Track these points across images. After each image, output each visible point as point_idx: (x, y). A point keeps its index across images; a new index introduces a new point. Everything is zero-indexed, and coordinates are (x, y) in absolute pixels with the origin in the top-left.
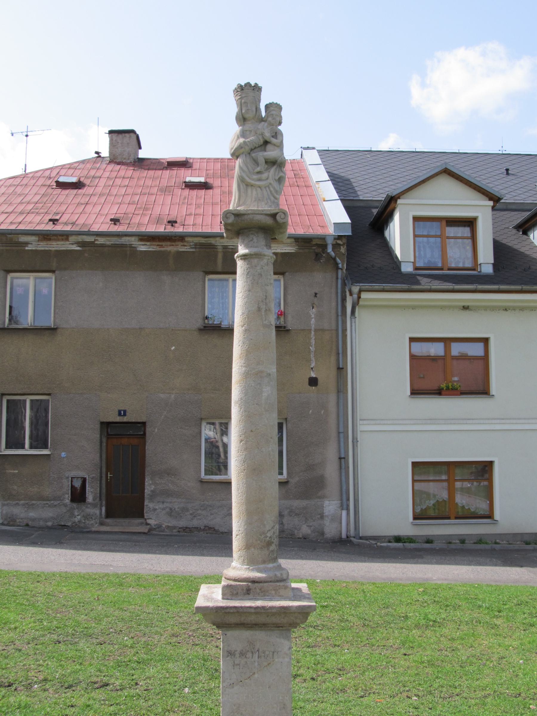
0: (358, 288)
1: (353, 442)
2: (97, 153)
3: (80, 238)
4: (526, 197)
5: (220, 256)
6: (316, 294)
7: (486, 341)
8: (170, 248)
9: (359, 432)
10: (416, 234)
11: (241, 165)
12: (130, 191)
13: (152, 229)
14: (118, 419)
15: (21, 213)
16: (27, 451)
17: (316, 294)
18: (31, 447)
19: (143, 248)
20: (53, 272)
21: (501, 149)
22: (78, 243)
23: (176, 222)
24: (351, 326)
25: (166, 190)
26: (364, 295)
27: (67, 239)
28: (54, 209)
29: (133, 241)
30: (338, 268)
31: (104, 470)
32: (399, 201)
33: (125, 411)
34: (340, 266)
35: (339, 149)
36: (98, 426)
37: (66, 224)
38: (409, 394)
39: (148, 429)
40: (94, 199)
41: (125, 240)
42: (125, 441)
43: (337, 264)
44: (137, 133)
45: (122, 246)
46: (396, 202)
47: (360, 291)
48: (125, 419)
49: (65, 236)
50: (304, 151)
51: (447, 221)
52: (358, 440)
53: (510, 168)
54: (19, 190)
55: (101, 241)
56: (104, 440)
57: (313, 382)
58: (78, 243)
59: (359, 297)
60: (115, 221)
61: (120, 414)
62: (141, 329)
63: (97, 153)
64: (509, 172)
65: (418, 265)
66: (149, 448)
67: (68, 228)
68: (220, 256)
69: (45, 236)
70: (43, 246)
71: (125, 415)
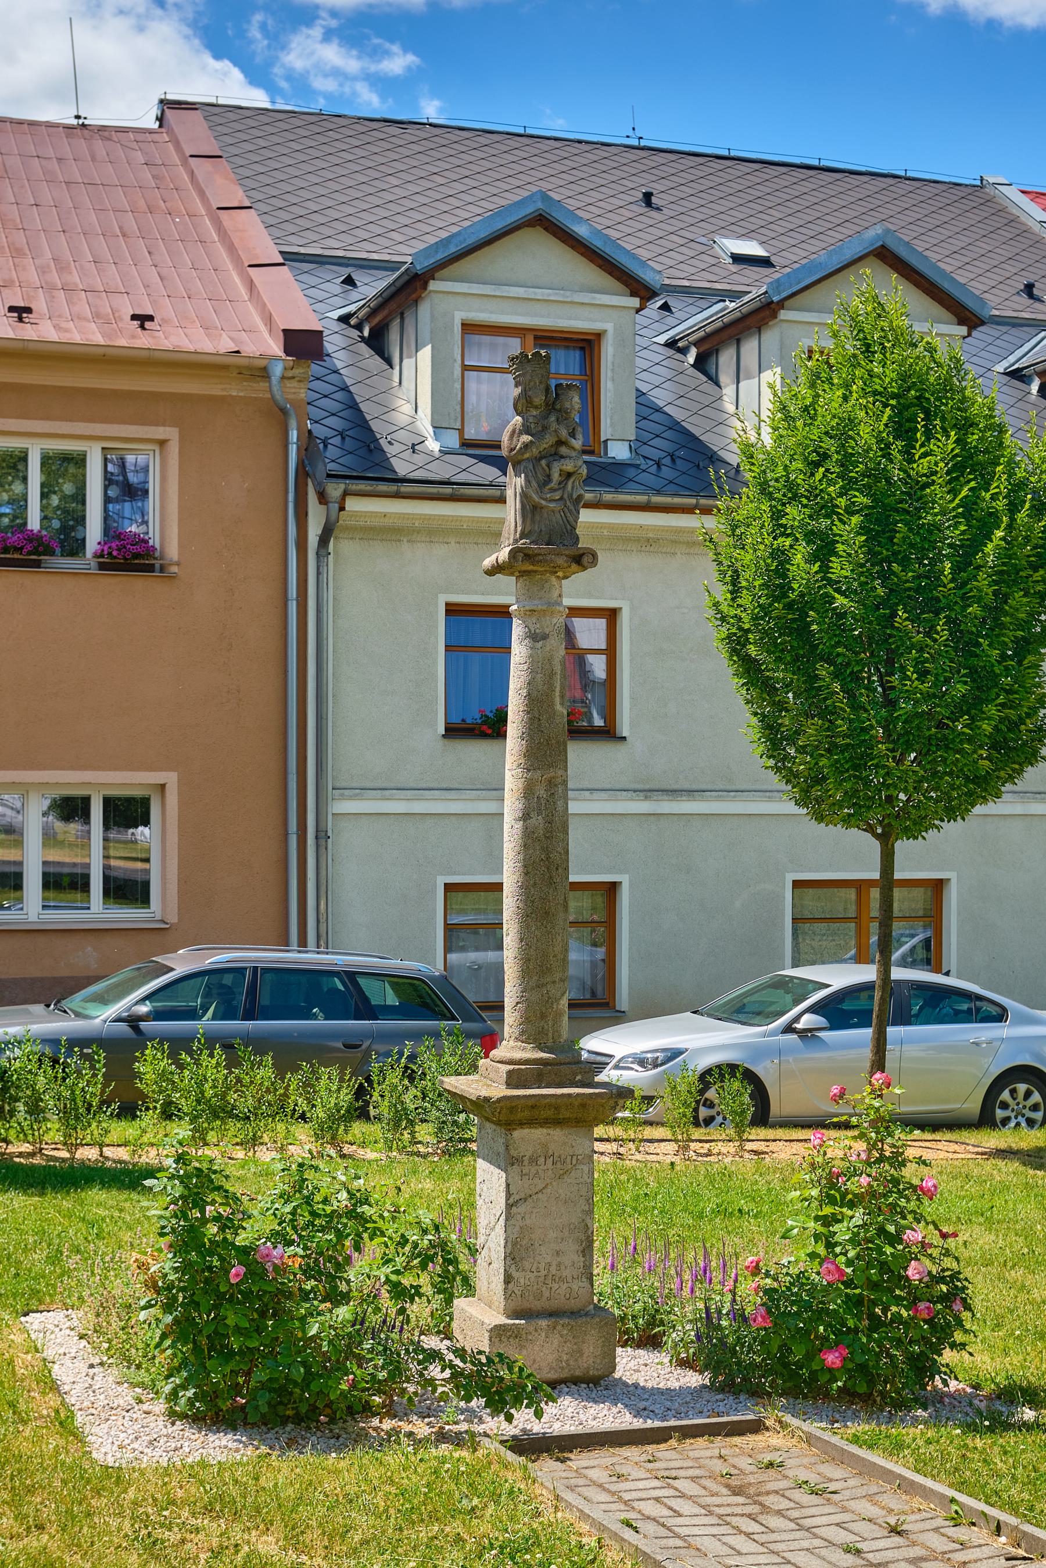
0: (342, 487)
1: (317, 838)
4: (693, 270)
7: (611, 615)
9: (330, 817)
10: (466, 363)
11: (518, 427)
21: (631, 133)
24: (318, 573)
26: (353, 505)
32: (433, 285)
35: (244, 104)
38: (442, 730)
46: (425, 286)
47: (346, 494)
50: (168, 112)
51: (536, 338)
52: (330, 834)
53: (656, 187)
59: (342, 508)
64: (654, 200)
65: (471, 433)
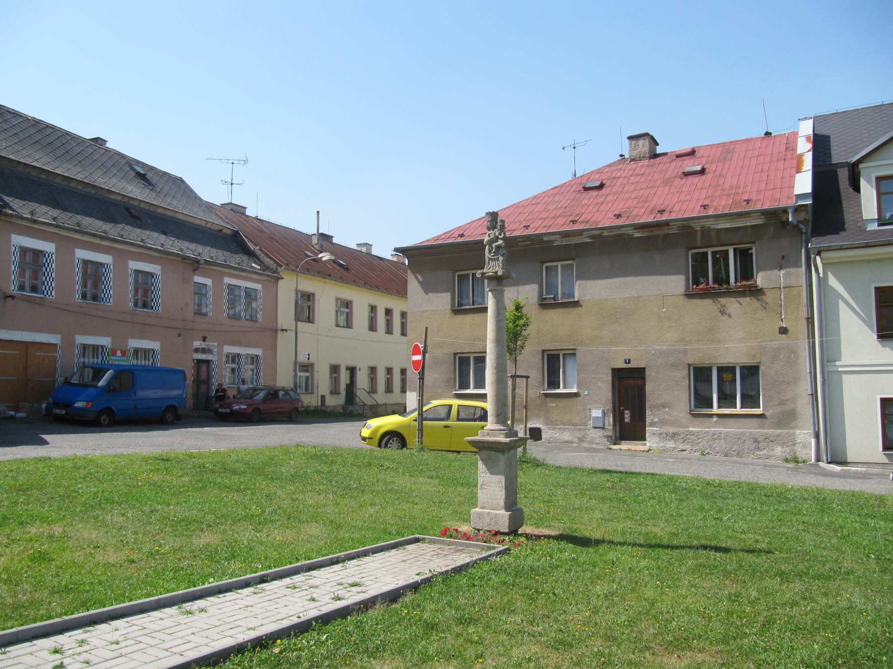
2: (621, 156)
3: (591, 233)
5: (699, 235)
6: (783, 257)
8: (660, 232)
12: (639, 186)
13: (644, 220)
14: (625, 366)
15: (553, 218)
16: (738, 410)
17: (783, 257)
18: (742, 407)
19: (637, 235)
20: (574, 259)
22: (590, 237)
23: (664, 211)
25: (668, 182)
27: (581, 234)
28: (577, 212)
29: (630, 231)
30: (802, 233)
31: (617, 404)
33: (629, 360)
34: (804, 230)
36: (610, 372)
37: (582, 222)
39: (647, 373)
40: (610, 198)
41: (622, 231)
42: (631, 382)
43: (801, 230)
44: (651, 134)
45: (622, 235)
48: (630, 366)
49: (580, 233)
54: (556, 199)
55: (606, 233)
56: (617, 382)
57: (784, 331)
58: (590, 237)
60: (618, 216)
61: (626, 362)
62: (638, 297)
63: (621, 156)
66: (649, 387)
67: (581, 227)
68: (699, 235)
69: (566, 235)
70: (566, 242)
71: (629, 362)
